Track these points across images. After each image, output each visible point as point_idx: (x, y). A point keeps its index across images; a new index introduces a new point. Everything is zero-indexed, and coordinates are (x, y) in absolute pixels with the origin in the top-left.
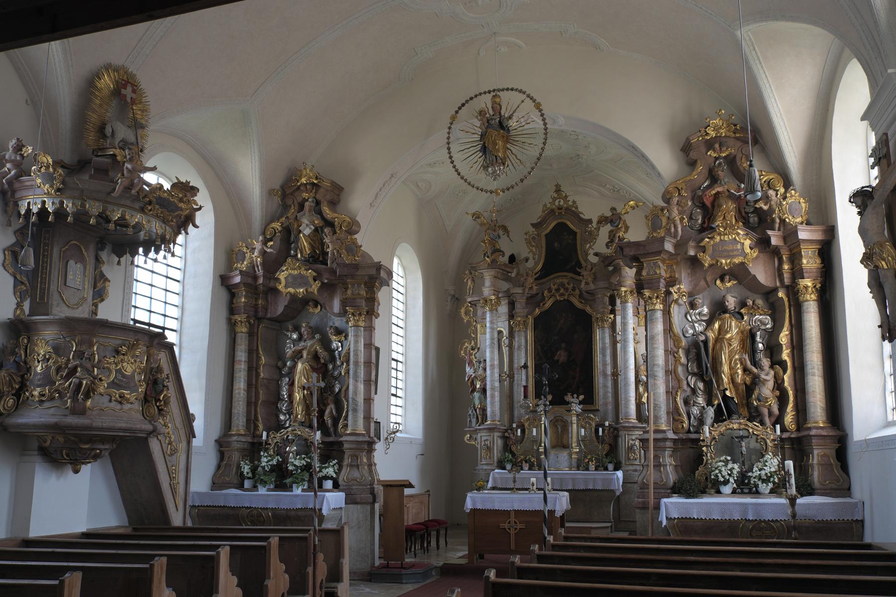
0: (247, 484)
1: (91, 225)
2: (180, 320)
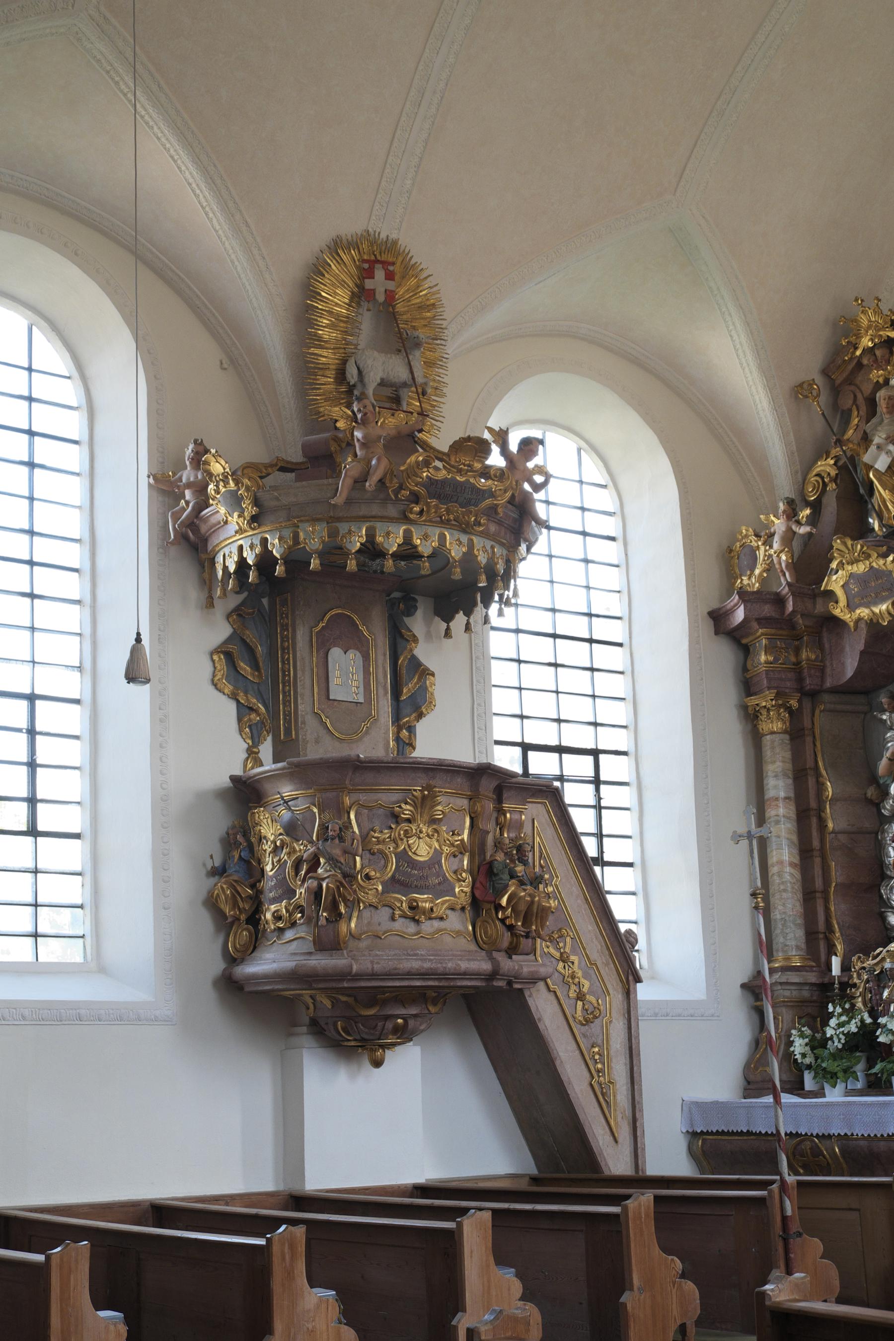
0: (809, 1082)
1: (314, 573)
2: (633, 727)
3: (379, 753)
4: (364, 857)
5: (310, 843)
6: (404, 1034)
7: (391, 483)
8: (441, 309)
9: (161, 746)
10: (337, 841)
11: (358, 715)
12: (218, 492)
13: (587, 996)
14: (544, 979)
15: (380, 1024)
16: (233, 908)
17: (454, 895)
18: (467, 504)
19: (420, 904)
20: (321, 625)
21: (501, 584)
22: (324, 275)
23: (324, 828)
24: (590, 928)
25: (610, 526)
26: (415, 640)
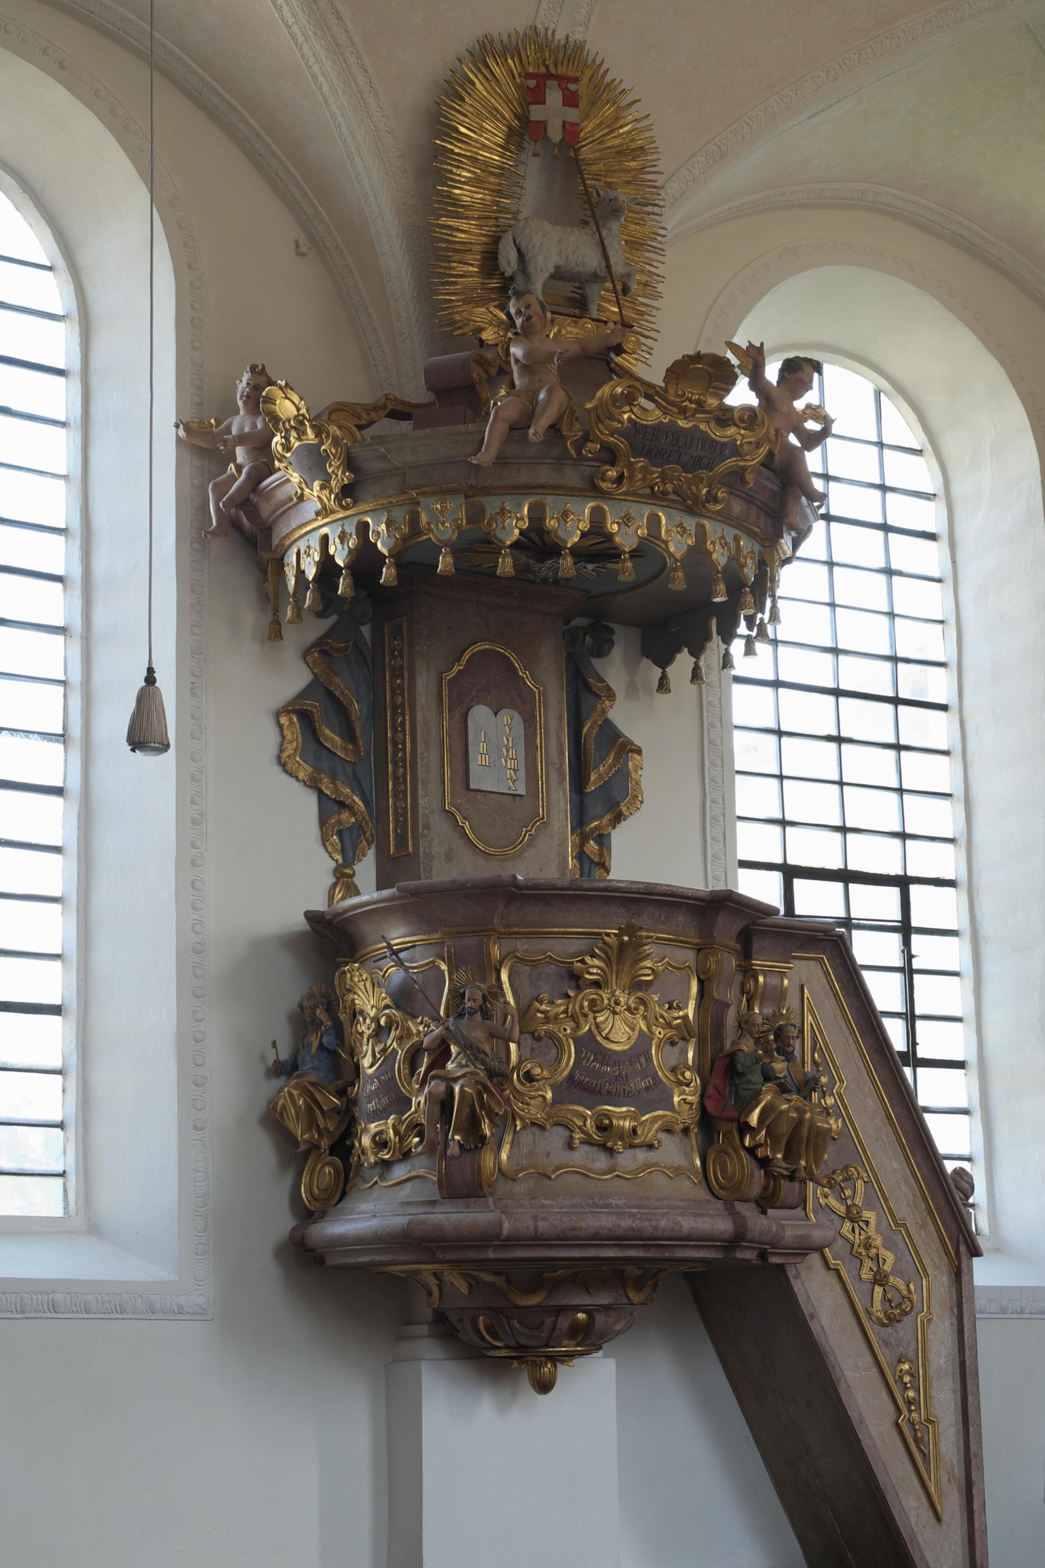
2: (965, 842)
3: (550, 873)
4: (523, 1044)
5: (434, 1020)
6: (588, 1339)
7: (571, 430)
8: (654, 157)
9: (194, 864)
10: (478, 1017)
11: (519, 813)
12: (287, 447)
13: (891, 1279)
14: (820, 1250)
15: (549, 1321)
16: (309, 1129)
17: (671, 1107)
18: (695, 465)
19: (615, 1122)
20: (457, 668)
21: (749, 599)
22: (463, 100)
23: (457, 996)
24: (895, 1165)
25: (928, 516)
26: (611, 695)
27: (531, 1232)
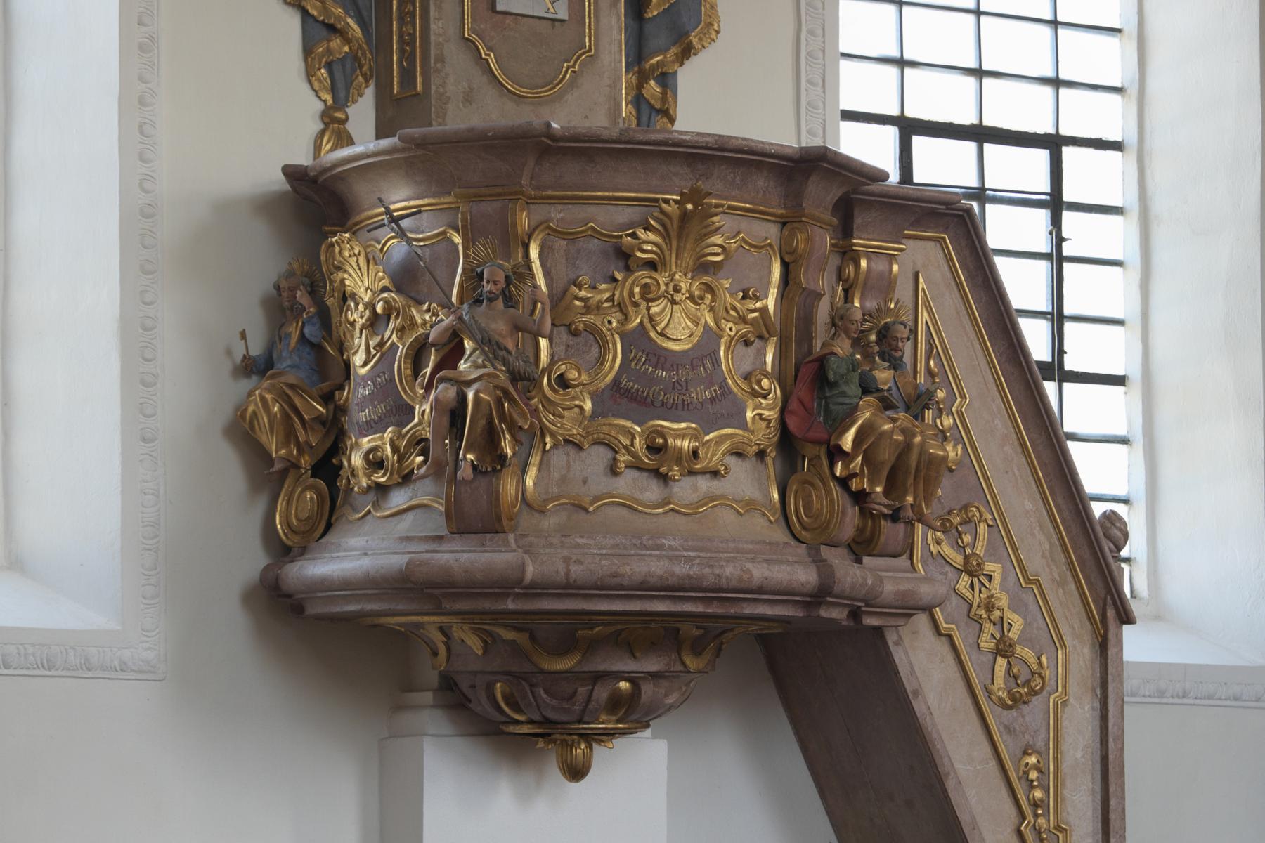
2: (1135, 92)
27: (561, 578)
